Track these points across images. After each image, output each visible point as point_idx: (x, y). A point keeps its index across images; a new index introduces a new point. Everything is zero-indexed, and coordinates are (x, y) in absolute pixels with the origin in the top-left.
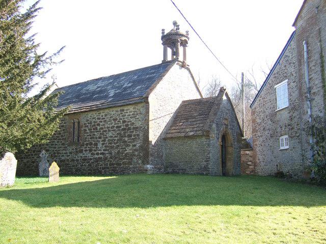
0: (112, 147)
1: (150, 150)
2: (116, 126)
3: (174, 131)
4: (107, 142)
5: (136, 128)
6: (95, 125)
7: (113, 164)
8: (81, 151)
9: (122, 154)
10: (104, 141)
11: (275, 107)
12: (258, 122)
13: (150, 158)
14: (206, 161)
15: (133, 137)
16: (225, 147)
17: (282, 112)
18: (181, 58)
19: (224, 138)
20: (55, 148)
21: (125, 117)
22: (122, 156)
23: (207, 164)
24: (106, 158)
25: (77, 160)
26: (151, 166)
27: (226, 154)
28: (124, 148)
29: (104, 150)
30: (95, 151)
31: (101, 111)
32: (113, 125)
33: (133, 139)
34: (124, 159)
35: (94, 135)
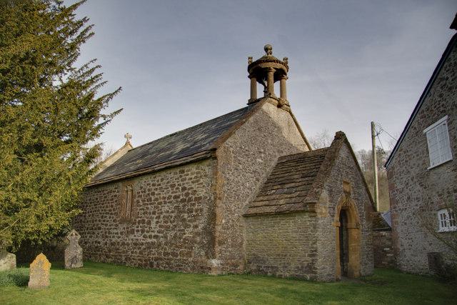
0: (168, 228)
1: (217, 234)
2: (173, 195)
3: (261, 203)
4: (161, 219)
5: (198, 199)
6: (148, 194)
7: (168, 254)
8: (132, 232)
9: (180, 238)
10: (159, 217)
11: (426, 163)
12: (398, 187)
13: (218, 248)
14: (310, 256)
15: (194, 213)
16: (347, 229)
17: (440, 170)
18: (277, 93)
19: (344, 214)
20: (106, 225)
21: (185, 182)
22: (180, 242)
23: (313, 260)
24: (160, 245)
25: (128, 244)
26: (219, 262)
27: (347, 239)
28: (183, 230)
29: (159, 232)
30: (148, 232)
31: (158, 174)
32: (170, 194)
33: (194, 216)
34: (181, 247)
35: (147, 208)
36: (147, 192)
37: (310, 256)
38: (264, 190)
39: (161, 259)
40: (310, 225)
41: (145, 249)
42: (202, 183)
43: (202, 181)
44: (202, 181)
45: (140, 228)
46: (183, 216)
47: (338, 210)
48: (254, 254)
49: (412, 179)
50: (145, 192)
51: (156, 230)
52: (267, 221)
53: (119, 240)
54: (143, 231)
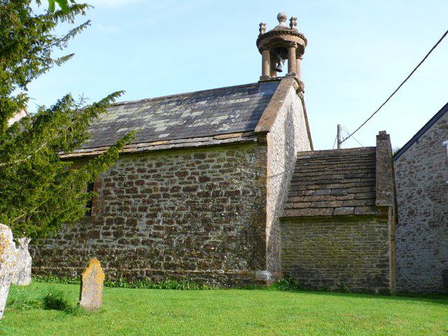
2: (183, 186)
6: (131, 183)
7: (174, 266)
14: (378, 266)
23: (383, 271)
32: (176, 184)
36: (127, 180)
37: (378, 266)
40: (379, 232)
45: (111, 230)
48: (296, 266)
49: (419, 192)
52: (316, 227)
53: (62, 248)
54: (117, 235)
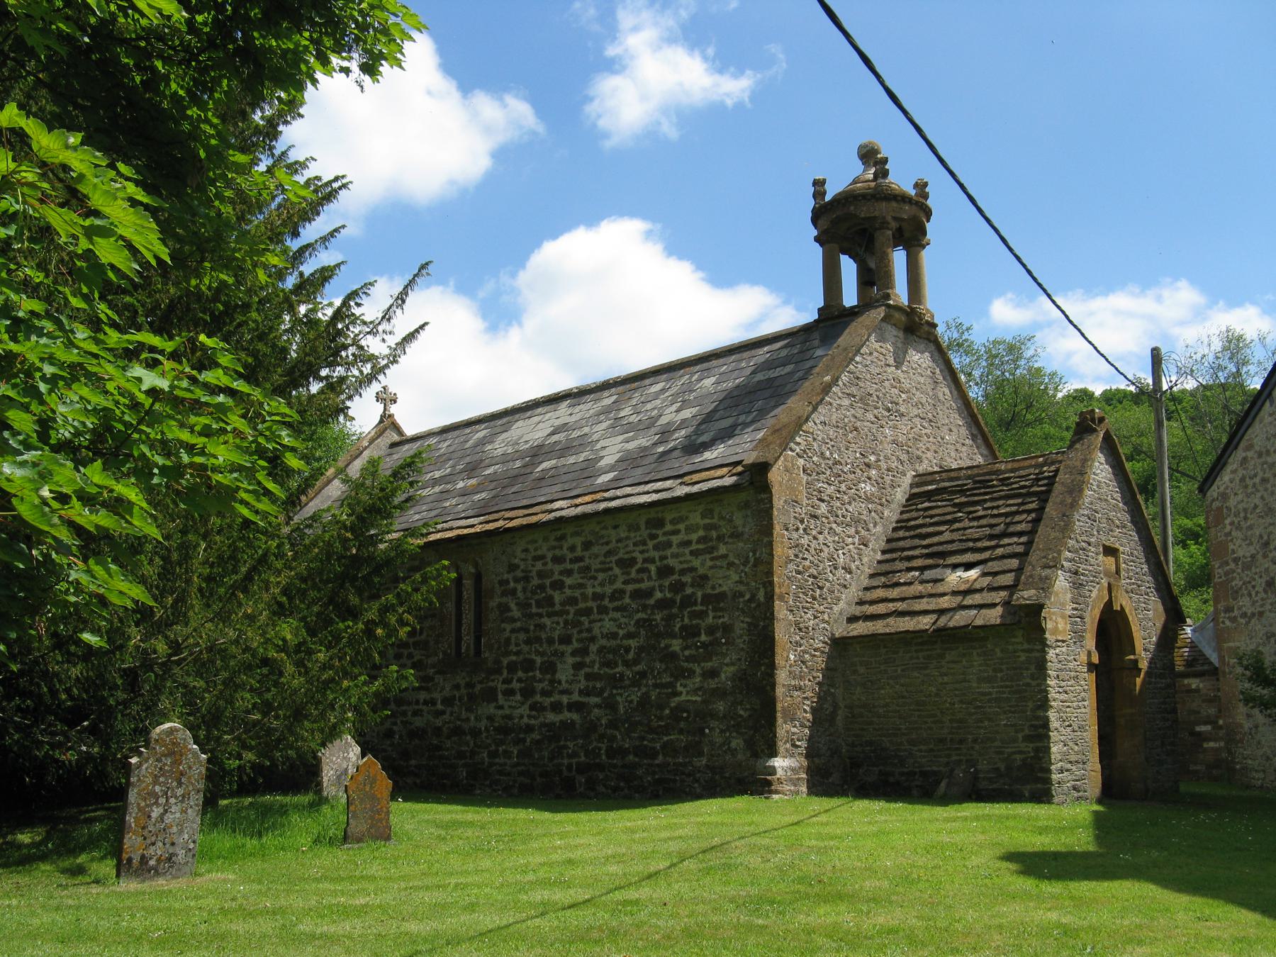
0: (616, 681)
2: (630, 588)
4: (592, 656)
5: (715, 600)
7: (623, 752)
8: (490, 695)
9: (661, 707)
10: (584, 652)
12: (1240, 553)
14: (1028, 738)
15: (703, 638)
21: (669, 552)
23: (1037, 750)
24: (592, 727)
25: (475, 733)
29: (586, 692)
30: (545, 693)
33: (704, 645)
34: (666, 730)
35: (541, 627)
36: (536, 581)
37: (1028, 738)
38: (883, 574)
39: (600, 767)
41: (538, 742)
42: (725, 556)
43: (723, 550)
44: (723, 550)
45: (515, 685)
46: (668, 646)
47: (1093, 619)
50: (527, 579)
51: (576, 688)
53: (439, 722)
54: (527, 692)
